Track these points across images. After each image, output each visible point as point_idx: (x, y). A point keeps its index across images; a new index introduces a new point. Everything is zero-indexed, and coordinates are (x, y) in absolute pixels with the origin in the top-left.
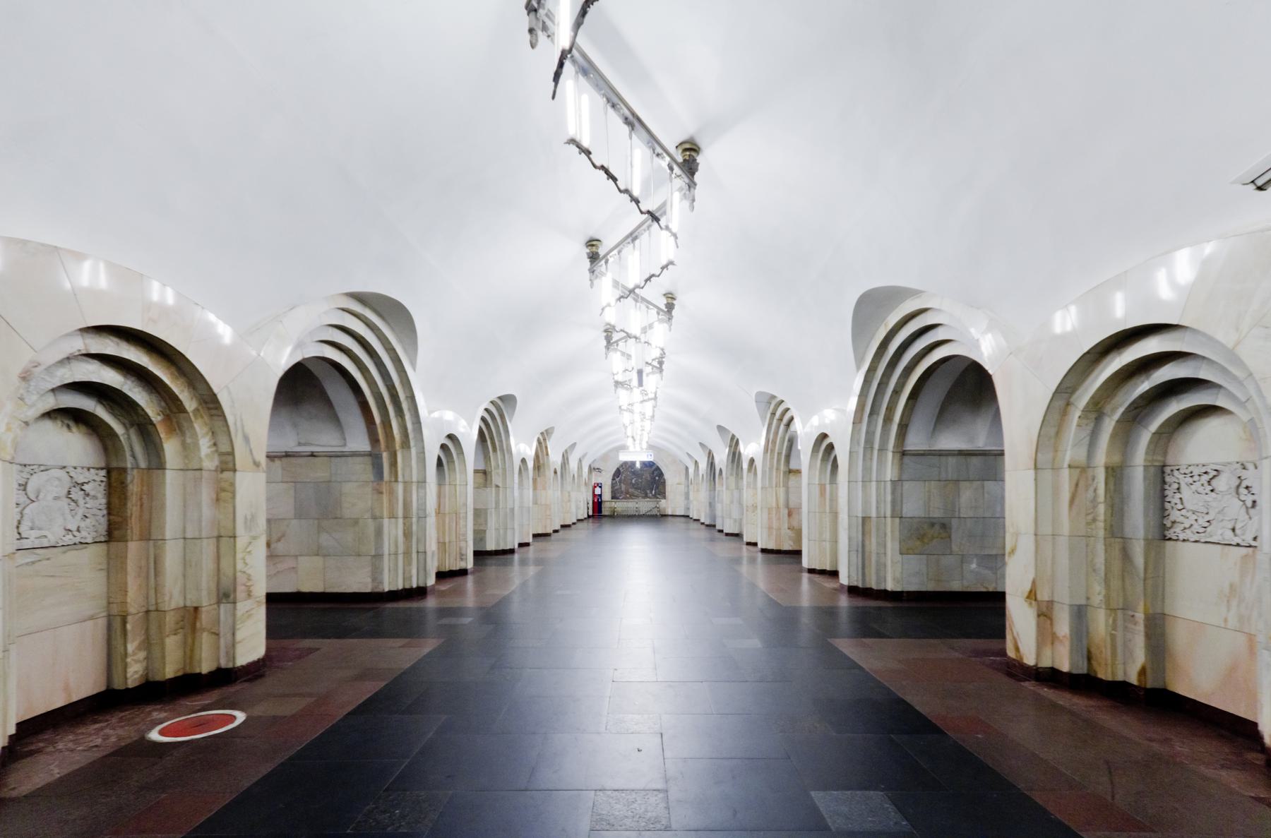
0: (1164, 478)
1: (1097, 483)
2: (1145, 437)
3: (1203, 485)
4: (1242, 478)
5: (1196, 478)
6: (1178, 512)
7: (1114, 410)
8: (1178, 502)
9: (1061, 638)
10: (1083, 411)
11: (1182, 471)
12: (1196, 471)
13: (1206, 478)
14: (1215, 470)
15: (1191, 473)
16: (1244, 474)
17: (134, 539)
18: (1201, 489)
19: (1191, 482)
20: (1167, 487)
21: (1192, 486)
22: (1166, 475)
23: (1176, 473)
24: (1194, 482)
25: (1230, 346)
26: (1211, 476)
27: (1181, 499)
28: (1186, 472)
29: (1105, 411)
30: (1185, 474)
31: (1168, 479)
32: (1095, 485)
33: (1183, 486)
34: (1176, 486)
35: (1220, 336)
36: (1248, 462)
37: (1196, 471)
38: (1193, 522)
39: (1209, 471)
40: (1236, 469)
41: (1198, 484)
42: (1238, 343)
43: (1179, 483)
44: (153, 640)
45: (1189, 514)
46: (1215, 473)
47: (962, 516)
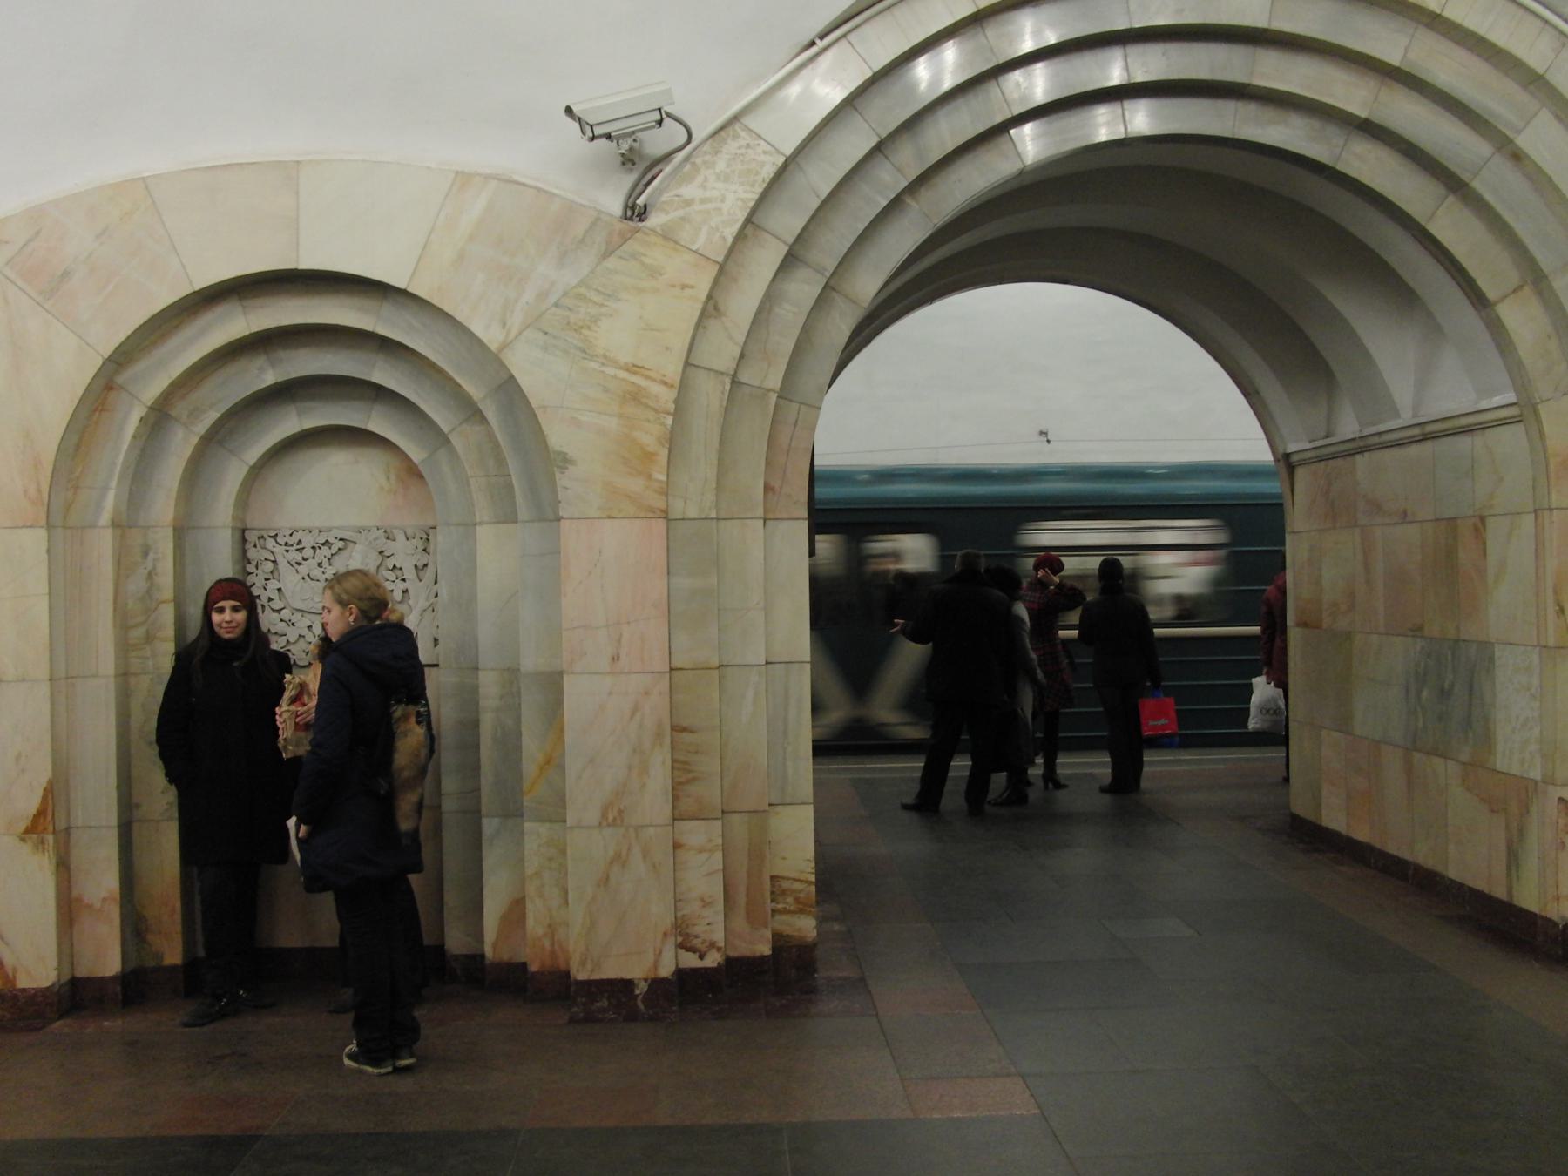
0: (244, 551)
1: (155, 560)
2: (234, 473)
3: (320, 565)
4: (386, 554)
5: (308, 553)
6: (275, 615)
7: (195, 413)
8: (275, 596)
9: (98, 905)
10: (151, 408)
11: (281, 540)
12: (308, 541)
13: (325, 551)
14: (341, 539)
15: (300, 542)
16: (390, 547)
17: (520, 517)
18: (317, 573)
19: (299, 559)
20: (250, 568)
21: (300, 568)
22: (248, 546)
23: (270, 543)
24: (304, 559)
25: (493, 347)
26: (335, 549)
27: (279, 590)
28: (291, 543)
29: (173, 413)
30: (286, 544)
31: (252, 553)
32: (149, 565)
33: (283, 565)
34: (270, 566)
35: (477, 328)
36: (396, 528)
37: (308, 541)
38: (305, 632)
39: (331, 540)
40: (376, 539)
41: (313, 563)
42: (505, 346)
43: (274, 562)
44: (1146, 731)
45: (297, 617)
46: (341, 544)
47: (1554, 506)
